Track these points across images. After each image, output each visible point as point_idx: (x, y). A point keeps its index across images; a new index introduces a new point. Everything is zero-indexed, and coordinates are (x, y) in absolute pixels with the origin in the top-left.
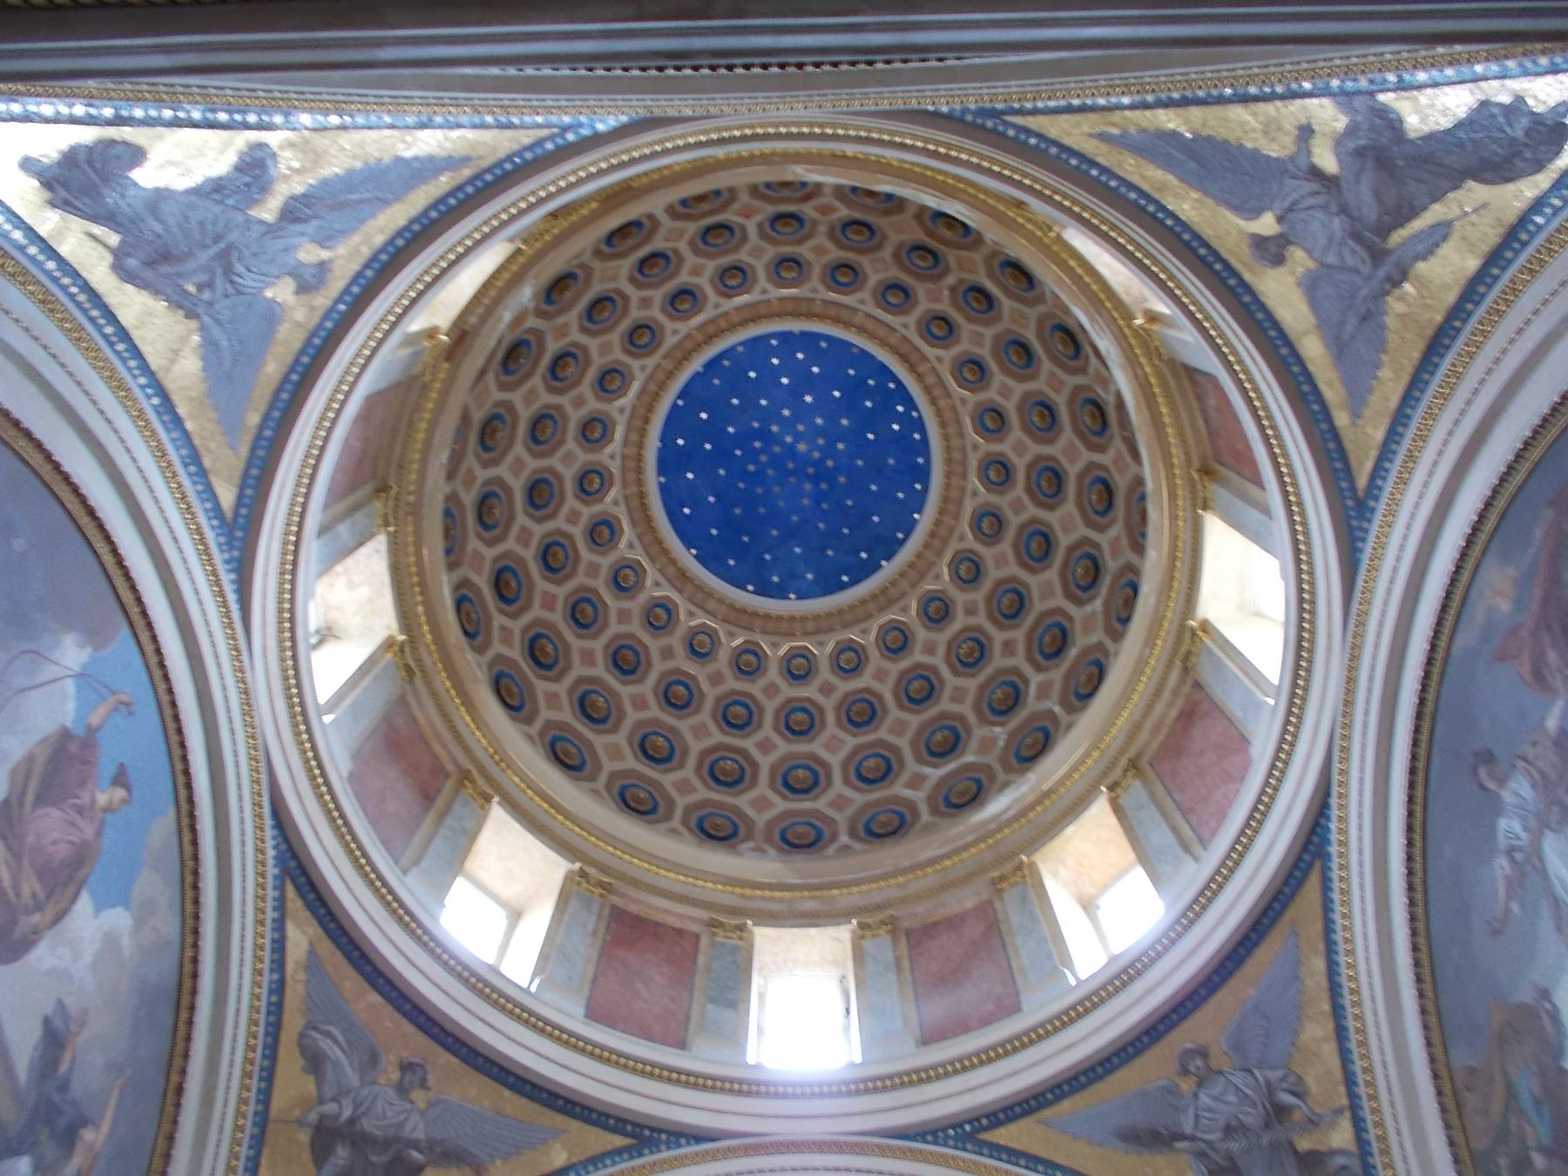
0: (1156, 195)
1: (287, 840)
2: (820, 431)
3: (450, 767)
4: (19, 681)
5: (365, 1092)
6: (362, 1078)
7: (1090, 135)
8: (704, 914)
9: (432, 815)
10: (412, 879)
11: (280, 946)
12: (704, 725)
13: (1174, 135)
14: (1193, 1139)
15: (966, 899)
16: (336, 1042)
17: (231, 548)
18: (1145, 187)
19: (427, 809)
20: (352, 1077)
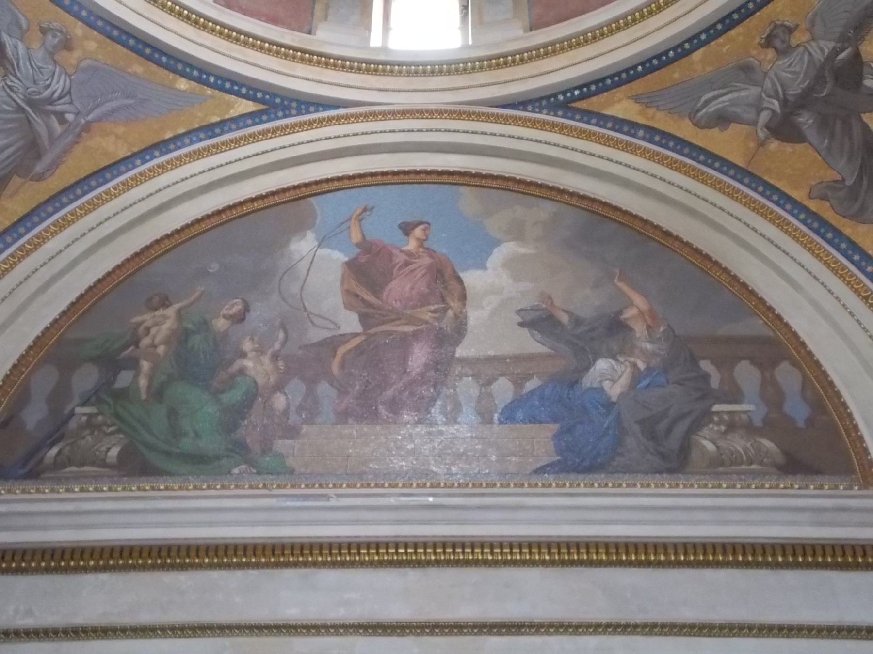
4: (295, 288)
6: (756, 84)
11: (619, 124)
16: (715, 98)
20: (751, 92)
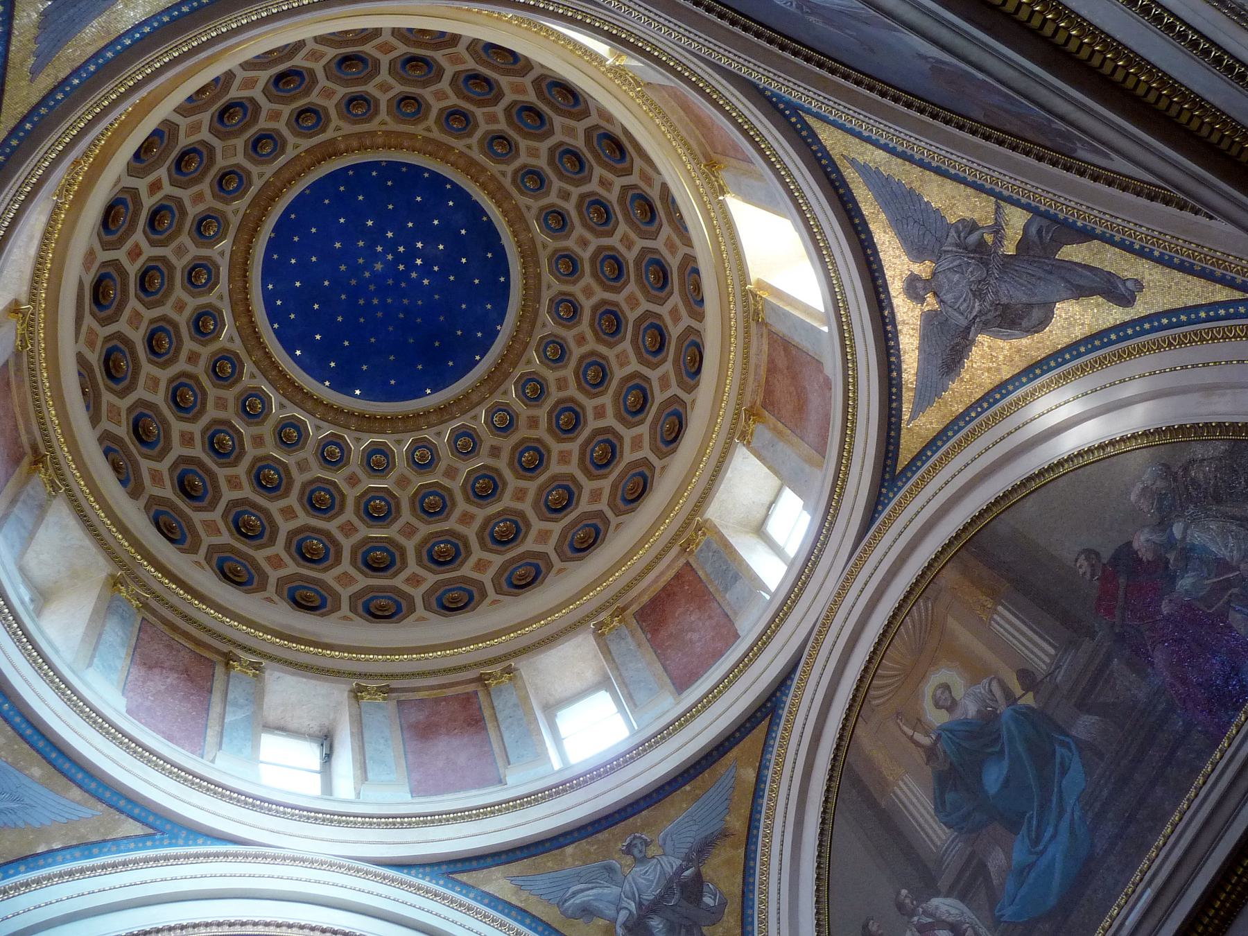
0: (112, 37)
1: (423, 865)
2: (371, 247)
3: (471, 688)
5: (627, 887)
7: (32, 81)
8: (675, 550)
9: (490, 726)
10: (511, 779)
12: (561, 452)
13: (45, 14)
14: (973, 321)
15: (760, 348)
16: (583, 891)
17: (176, 837)
18: (102, 44)
19: (485, 728)
